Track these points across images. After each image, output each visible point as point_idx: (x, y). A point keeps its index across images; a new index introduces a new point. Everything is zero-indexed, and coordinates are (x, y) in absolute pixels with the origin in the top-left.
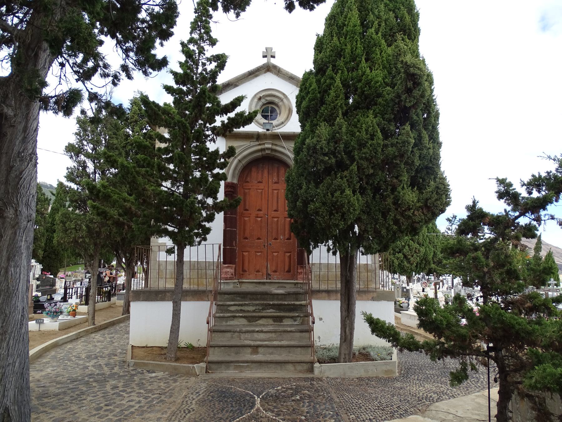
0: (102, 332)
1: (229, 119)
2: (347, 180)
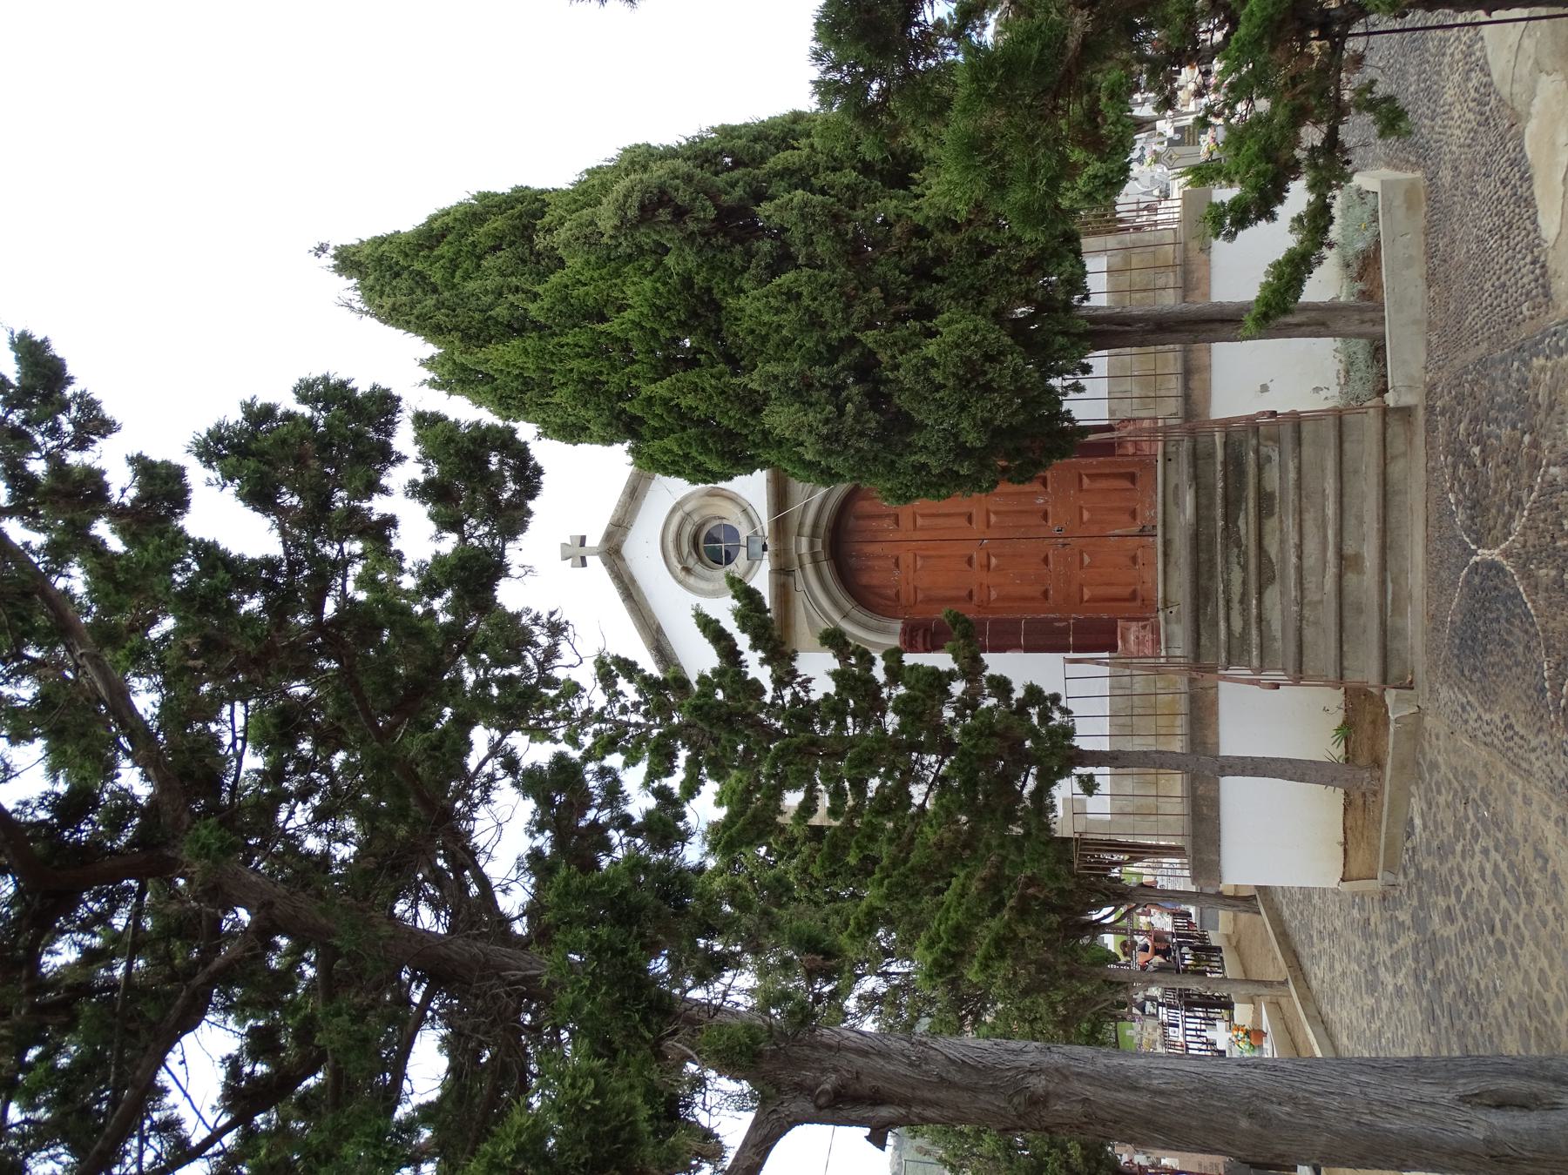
0: (1307, 963)
1: (754, 647)
2: (902, 352)
